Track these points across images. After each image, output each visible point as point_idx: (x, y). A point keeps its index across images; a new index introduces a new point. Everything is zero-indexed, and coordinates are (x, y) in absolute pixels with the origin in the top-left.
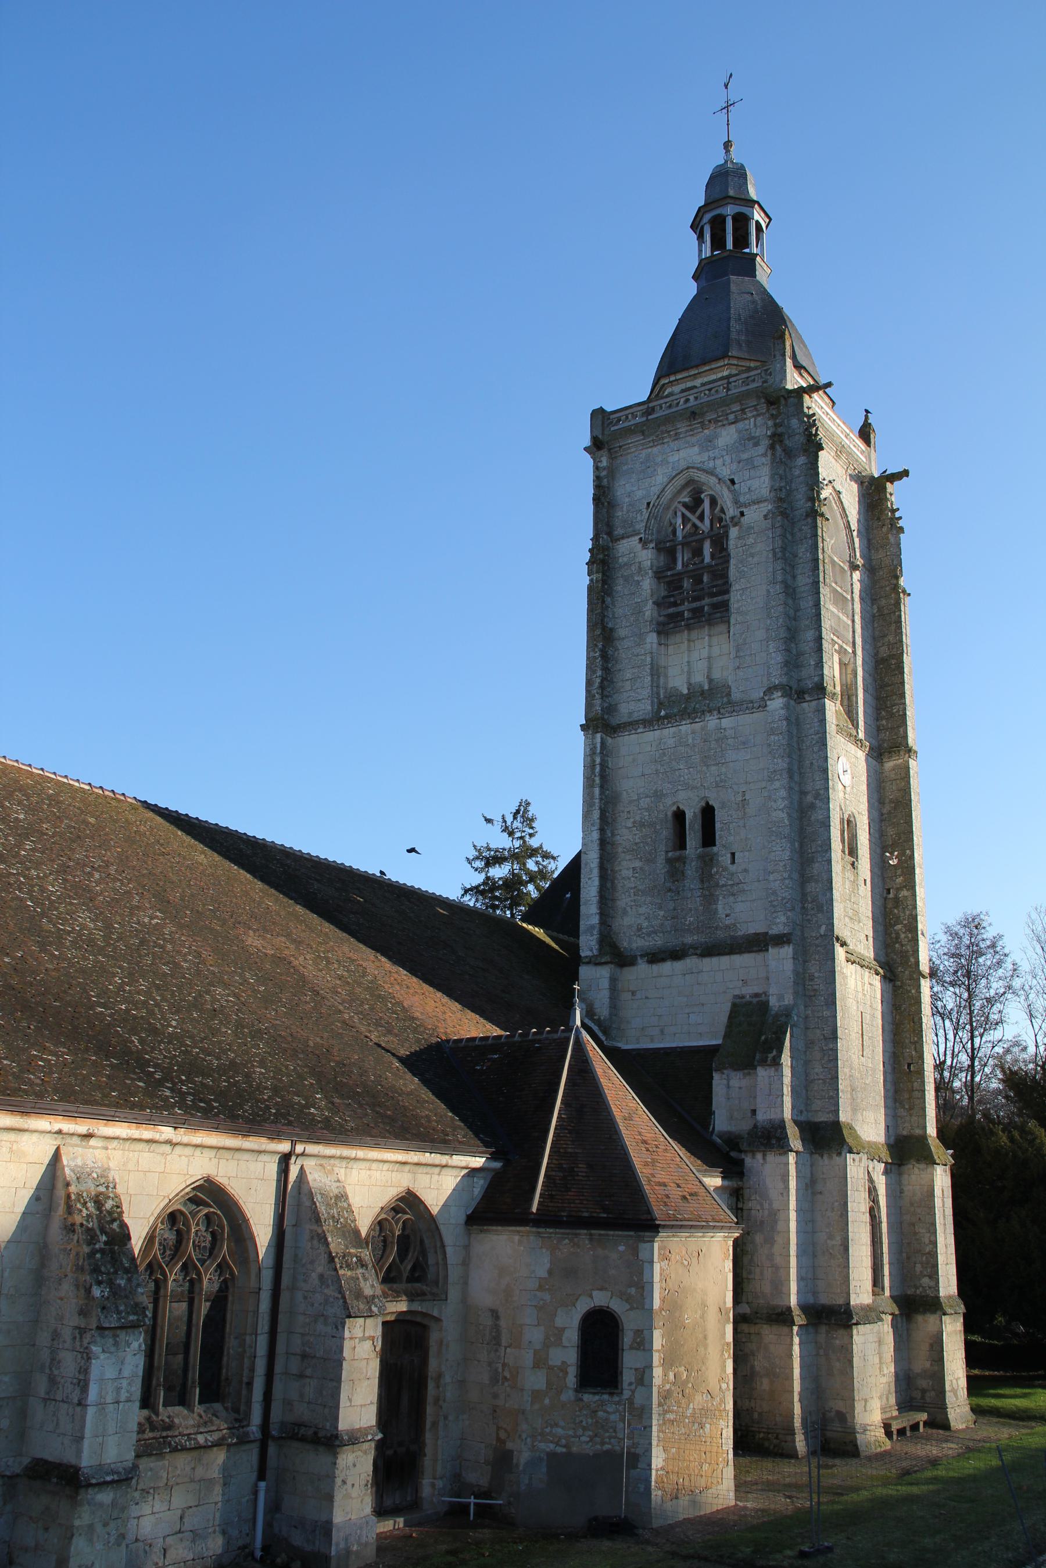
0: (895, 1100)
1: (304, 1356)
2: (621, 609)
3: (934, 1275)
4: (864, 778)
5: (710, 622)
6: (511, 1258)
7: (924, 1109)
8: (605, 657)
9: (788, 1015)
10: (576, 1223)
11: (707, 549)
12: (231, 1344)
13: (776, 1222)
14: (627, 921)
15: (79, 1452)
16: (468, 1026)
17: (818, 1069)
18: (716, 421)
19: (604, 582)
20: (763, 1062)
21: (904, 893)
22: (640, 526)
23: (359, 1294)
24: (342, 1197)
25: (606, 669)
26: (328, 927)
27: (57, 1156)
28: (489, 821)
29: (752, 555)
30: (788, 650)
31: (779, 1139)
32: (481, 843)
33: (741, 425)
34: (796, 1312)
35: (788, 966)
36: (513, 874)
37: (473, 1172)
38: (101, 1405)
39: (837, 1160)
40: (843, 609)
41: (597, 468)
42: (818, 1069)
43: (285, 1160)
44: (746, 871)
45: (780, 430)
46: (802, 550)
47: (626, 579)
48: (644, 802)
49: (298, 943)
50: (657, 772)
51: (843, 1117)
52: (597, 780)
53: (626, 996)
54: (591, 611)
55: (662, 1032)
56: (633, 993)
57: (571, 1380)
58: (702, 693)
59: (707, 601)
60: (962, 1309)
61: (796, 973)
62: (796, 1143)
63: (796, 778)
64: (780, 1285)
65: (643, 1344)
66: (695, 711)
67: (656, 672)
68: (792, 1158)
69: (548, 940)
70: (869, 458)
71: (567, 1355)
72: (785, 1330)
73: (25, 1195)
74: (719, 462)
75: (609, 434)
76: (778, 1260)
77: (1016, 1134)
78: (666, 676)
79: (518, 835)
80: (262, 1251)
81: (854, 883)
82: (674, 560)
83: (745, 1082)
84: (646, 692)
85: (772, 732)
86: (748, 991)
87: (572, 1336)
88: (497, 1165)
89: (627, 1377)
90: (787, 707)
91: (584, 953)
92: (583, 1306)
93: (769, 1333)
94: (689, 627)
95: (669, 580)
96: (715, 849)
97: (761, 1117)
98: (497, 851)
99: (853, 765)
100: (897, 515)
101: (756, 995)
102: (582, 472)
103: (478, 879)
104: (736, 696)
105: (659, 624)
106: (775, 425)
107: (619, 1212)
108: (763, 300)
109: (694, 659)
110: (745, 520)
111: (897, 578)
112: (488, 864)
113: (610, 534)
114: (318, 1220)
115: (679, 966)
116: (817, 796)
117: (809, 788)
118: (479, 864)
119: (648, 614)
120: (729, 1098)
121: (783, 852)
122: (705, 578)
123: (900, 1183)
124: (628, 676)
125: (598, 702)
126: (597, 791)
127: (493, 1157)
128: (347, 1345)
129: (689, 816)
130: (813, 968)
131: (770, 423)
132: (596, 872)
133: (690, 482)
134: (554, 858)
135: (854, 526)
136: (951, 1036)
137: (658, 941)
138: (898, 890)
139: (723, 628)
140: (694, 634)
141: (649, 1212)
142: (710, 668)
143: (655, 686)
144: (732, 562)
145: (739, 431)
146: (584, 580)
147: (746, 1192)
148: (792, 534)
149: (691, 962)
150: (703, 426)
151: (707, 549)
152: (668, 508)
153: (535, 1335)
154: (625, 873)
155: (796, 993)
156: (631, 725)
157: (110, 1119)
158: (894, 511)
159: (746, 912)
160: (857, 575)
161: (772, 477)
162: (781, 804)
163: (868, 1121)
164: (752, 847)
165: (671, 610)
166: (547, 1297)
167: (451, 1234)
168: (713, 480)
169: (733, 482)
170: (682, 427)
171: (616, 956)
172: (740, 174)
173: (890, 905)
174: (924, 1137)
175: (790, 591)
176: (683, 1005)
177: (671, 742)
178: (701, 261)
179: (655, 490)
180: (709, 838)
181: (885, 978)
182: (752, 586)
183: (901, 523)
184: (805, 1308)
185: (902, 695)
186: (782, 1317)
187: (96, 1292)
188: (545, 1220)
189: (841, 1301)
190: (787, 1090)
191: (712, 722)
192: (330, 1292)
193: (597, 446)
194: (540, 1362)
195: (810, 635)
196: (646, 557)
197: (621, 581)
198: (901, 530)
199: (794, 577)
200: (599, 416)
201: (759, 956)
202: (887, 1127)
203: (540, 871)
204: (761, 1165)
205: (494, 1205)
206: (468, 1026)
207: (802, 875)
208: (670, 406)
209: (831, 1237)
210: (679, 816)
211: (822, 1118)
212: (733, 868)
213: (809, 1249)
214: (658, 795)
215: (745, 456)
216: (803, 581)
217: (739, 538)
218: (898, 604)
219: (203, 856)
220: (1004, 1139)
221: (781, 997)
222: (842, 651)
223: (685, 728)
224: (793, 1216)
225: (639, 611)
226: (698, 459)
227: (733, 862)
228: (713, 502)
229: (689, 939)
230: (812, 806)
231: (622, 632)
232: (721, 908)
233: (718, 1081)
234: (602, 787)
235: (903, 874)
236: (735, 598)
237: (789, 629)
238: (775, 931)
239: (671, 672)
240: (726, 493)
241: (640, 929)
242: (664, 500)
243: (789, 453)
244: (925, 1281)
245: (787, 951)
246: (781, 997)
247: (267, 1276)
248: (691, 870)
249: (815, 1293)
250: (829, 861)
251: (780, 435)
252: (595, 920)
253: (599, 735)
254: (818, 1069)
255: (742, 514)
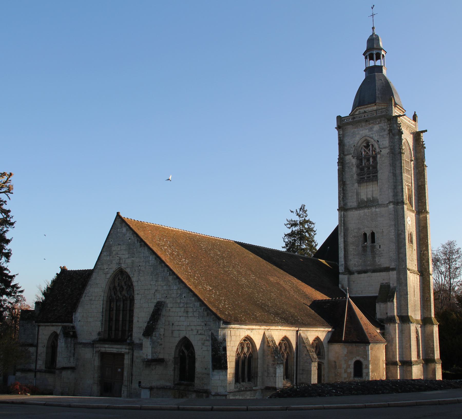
0: (423, 308)
1: (303, 370)
2: (347, 176)
3: (433, 353)
4: (414, 221)
5: (372, 181)
6: (338, 350)
7: (431, 310)
8: (343, 190)
9: (395, 289)
10: (352, 342)
11: (371, 160)
12: (289, 368)
13: (393, 341)
14: (352, 262)
15: (276, 385)
16: (320, 296)
17: (403, 302)
18: (373, 123)
19: (342, 168)
20: (389, 301)
21: (426, 252)
22: (352, 152)
23: (313, 357)
24: (307, 338)
25: (344, 193)
26: (282, 271)
27: (264, 333)
28: (292, 212)
29: (384, 163)
30: (394, 192)
31: (393, 320)
32: (289, 219)
33: (380, 125)
34: (398, 362)
35: (395, 276)
36: (300, 229)
37: (329, 332)
38: (278, 377)
39: (408, 325)
40: (409, 174)
41: (339, 135)
42: (403, 302)
43: (297, 331)
44: (383, 250)
45: (391, 128)
46: (398, 163)
47: (349, 167)
48: (356, 231)
49: (279, 277)
50: (359, 223)
51: (409, 314)
52: (343, 224)
53: (352, 282)
54: (339, 177)
55: (362, 292)
56: (354, 282)
57: (352, 375)
58: (371, 201)
59: (371, 175)
60: (441, 362)
61: (397, 278)
62: (398, 321)
63: (397, 226)
64: (394, 356)
65: (367, 367)
66: (369, 206)
67: (358, 194)
68: (397, 325)
69: (326, 264)
70: (415, 125)
71: (351, 370)
72: (396, 366)
73: (261, 340)
74: (374, 135)
75: (342, 124)
76: (394, 350)
77: (458, 315)
78: (360, 195)
79: (301, 216)
80: (294, 350)
81: (412, 251)
82: (362, 163)
83: (384, 306)
84: (355, 200)
85: (390, 214)
86: (384, 282)
87: (352, 366)
88: (333, 330)
89: (364, 374)
90: (394, 207)
91: (340, 271)
92: (354, 360)
93: (392, 368)
94: (366, 182)
95: (359, 166)
96: (375, 244)
97: (389, 315)
98: (294, 221)
99: (411, 218)
100: (424, 143)
101: (387, 283)
102: (335, 134)
103: (289, 231)
104: (380, 202)
105: (358, 180)
106: (390, 127)
107: (363, 340)
108: (385, 82)
109: (368, 191)
110: (382, 153)
111: (424, 162)
112: (292, 226)
113: (343, 154)
114: (304, 343)
115: (365, 275)
116: (402, 231)
117: (400, 229)
118: (289, 226)
119: (355, 178)
120: (380, 309)
121: (393, 247)
122: (371, 168)
123: (424, 330)
124: (350, 195)
125: (342, 203)
126: (342, 227)
127: (333, 328)
128: (312, 367)
129: (368, 235)
130: (402, 276)
131: (388, 126)
132: (343, 250)
133: (366, 140)
134: (313, 224)
135: (411, 148)
136: (443, 279)
137: (360, 268)
138: (424, 251)
139: (376, 182)
140: (368, 184)
141: (368, 339)
142: (372, 194)
143: (358, 198)
144: (378, 165)
145: (380, 127)
146: (336, 168)
147: (385, 333)
148: (395, 158)
149: (369, 274)
150: (369, 124)
151: (371, 160)
152: (360, 147)
153: (344, 366)
154: (350, 250)
155: (397, 283)
156: (351, 209)
157: (272, 326)
158: (423, 142)
159: (383, 261)
160: (412, 163)
161: (389, 142)
162: (393, 234)
163: (415, 313)
164: (385, 243)
165: (361, 177)
166: (347, 358)
167: (325, 345)
168: (372, 140)
169: (378, 141)
170: (363, 124)
171: (349, 272)
172: (377, 39)
173: (422, 255)
174: (431, 318)
175: (394, 175)
176: (368, 285)
177: (362, 214)
178: (366, 68)
179: (356, 142)
180: (373, 241)
181: (420, 276)
182: (384, 172)
183: (425, 146)
184: (400, 361)
185: (425, 197)
186: (395, 364)
187: (276, 357)
188: (346, 342)
189: (409, 360)
190: (395, 308)
191: (373, 209)
192: (308, 357)
193: (339, 128)
194: (346, 372)
195: (400, 187)
196: (354, 161)
197: (347, 168)
198: (425, 148)
199: (395, 171)
200: (339, 118)
201: (387, 273)
202: (421, 315)
203: (309, 228)
204: (389, 327)
205: (334, 338)
206: (320, 296)
207: (398, 252)
208: (360, 117)
209: (407, 344)
210: (365, 234)
211: (404, 314)
212: (380, 249)
213: (401, 347)
214: (359, 229)
215: (381, 134)
216: (398, 172)
217: (380, 158)
218: (424, 170)
219: (252, 256)
220: (454, 316)
221: (393, 284)
222: (408, 185)
223: (366, 210)
224: (397, 339)
225: (352, 177)
226: (368, 134)
227: (380, 248)
228: (373, 146)
229: (368, 268)
230: (401, 234)
231: (348, 182)
232: (377, 259)
233: (377, 306)
234: (344, 226)
235: (425, 247)
236: (379, 175)
237: (394, 186)
238: (391, 267)
239: (362, 194)
240: (376, 144)
241: (355, 265)
242: (359, 145)
243: (394, 135)
244: (431, 355)
245: (395, 272)
246: (393, 284)
247: (295, 354)
248: (369, 249)
249: (403, 358)
250: (405, 249)
251: (391, 130)
252: (343, 263)
253: (342, 212)
254: (403, 302)
255: (381, 151)
